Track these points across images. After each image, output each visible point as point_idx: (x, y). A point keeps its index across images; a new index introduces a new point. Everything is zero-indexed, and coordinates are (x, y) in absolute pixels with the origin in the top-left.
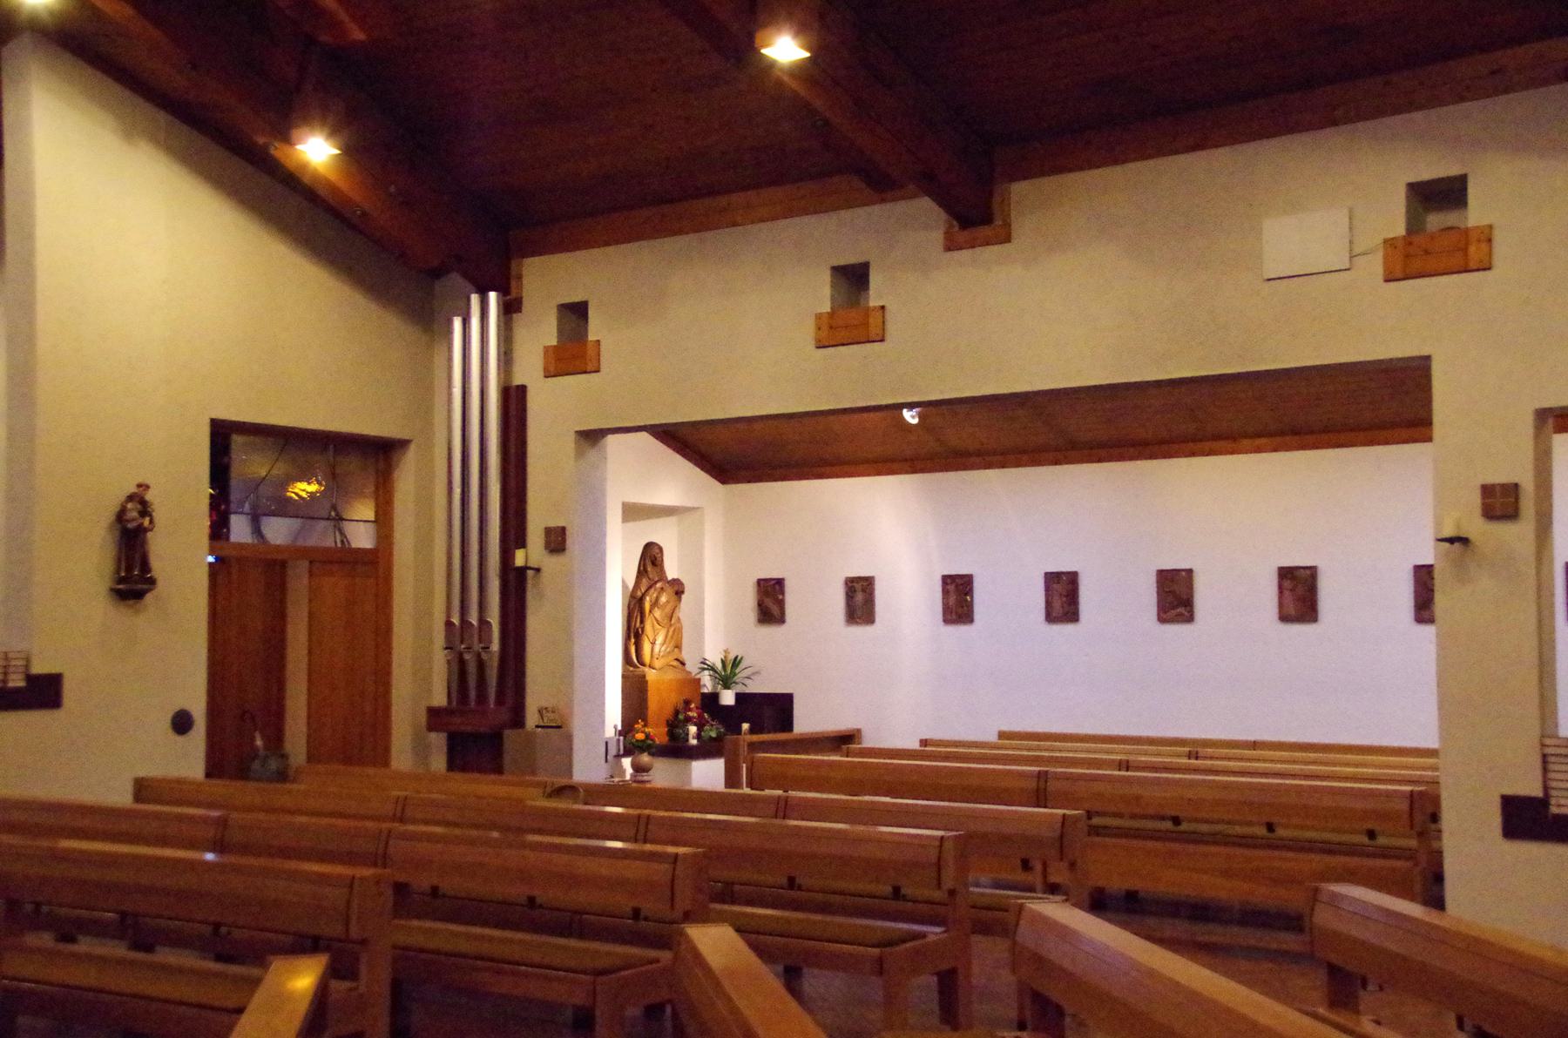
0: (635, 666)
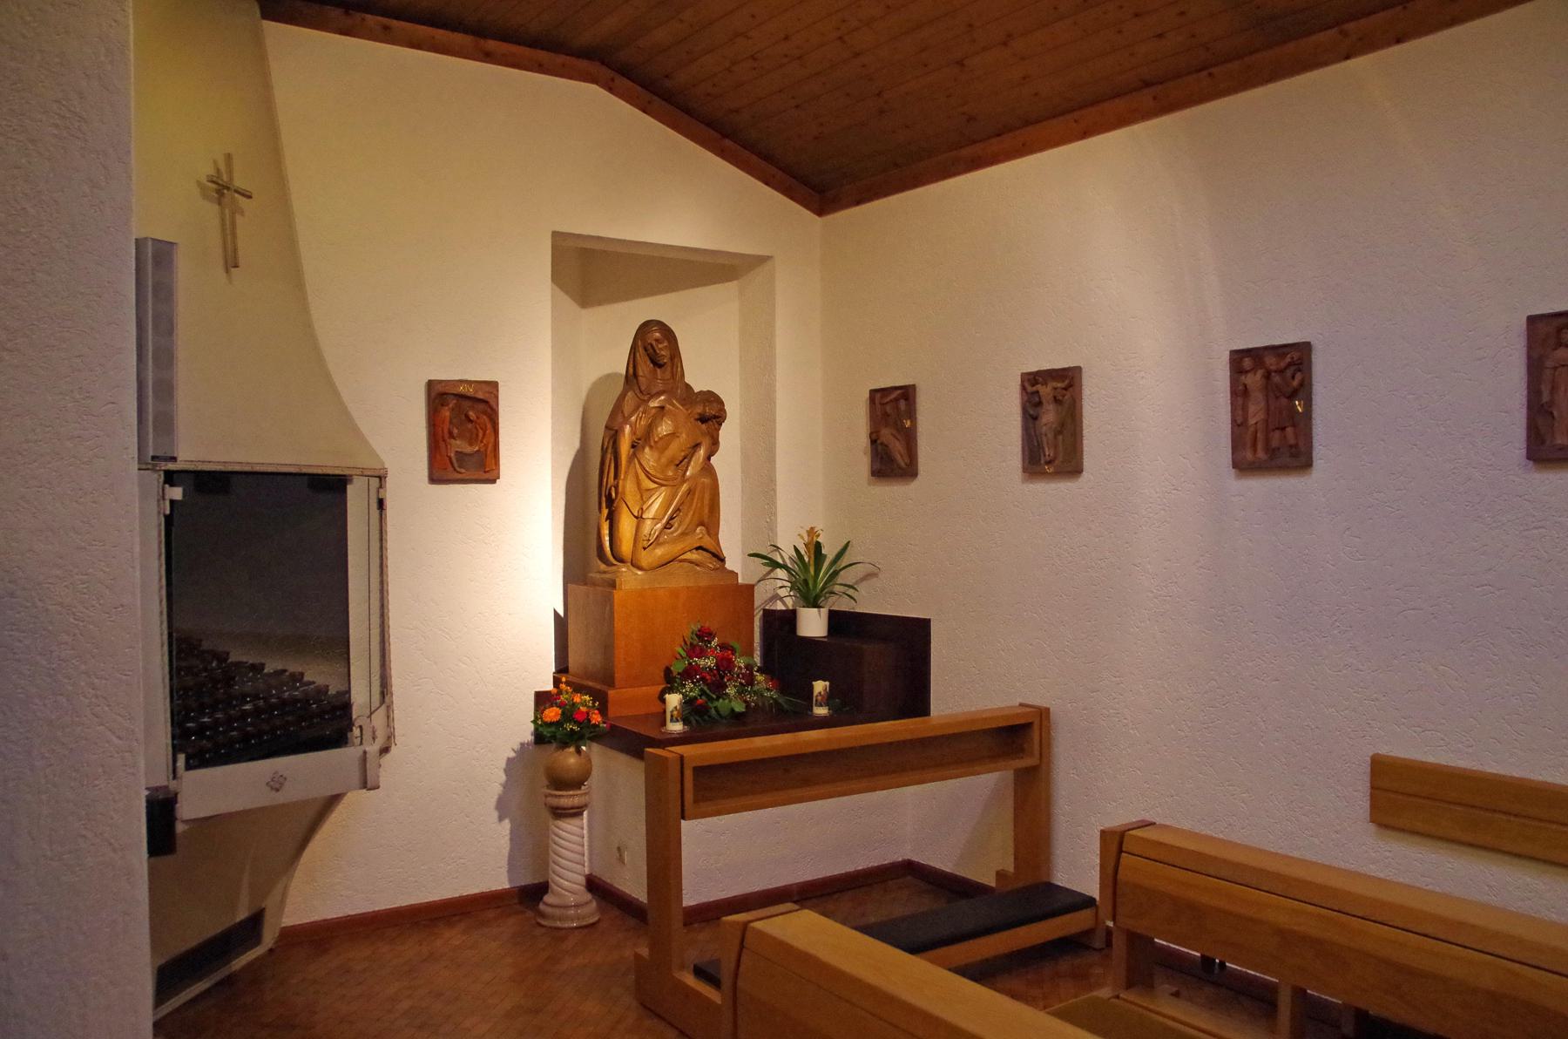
0: (609, 564)
